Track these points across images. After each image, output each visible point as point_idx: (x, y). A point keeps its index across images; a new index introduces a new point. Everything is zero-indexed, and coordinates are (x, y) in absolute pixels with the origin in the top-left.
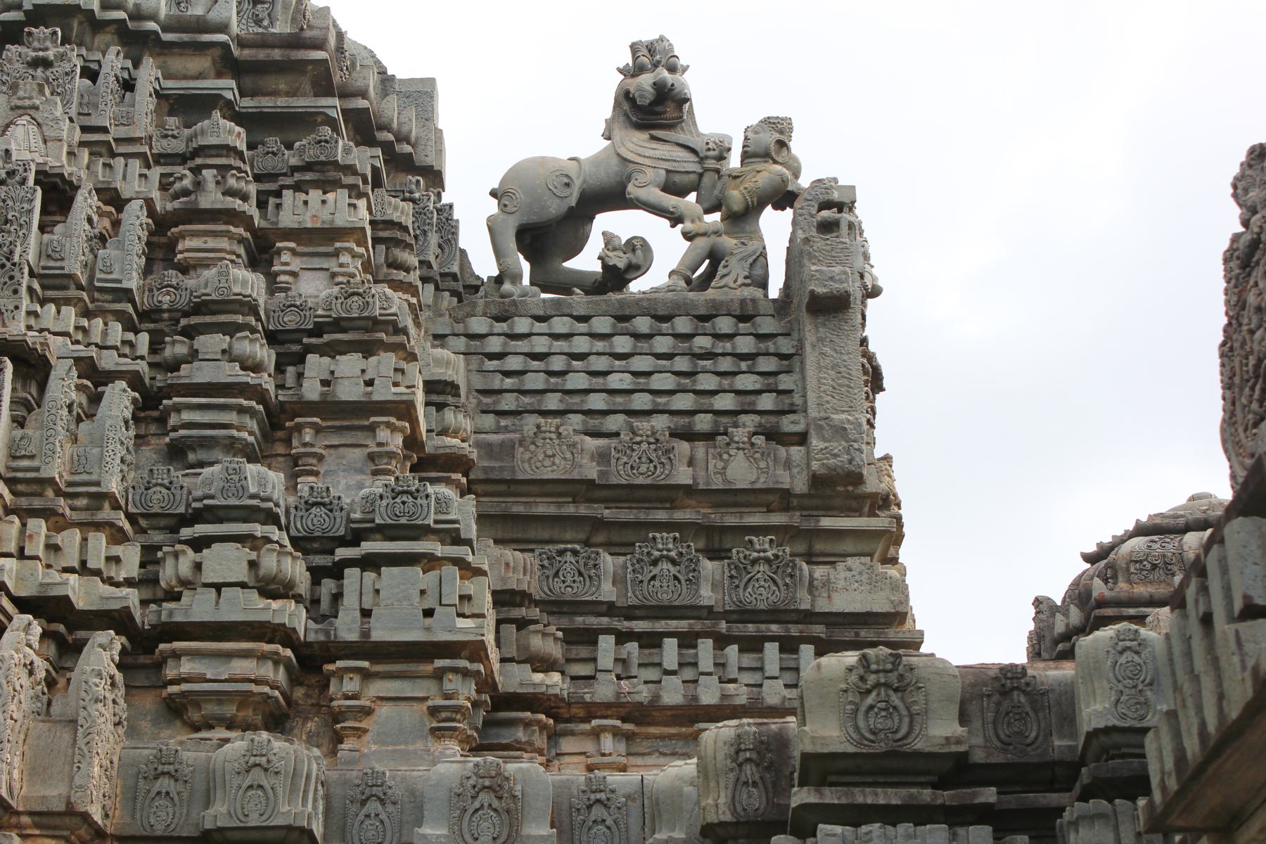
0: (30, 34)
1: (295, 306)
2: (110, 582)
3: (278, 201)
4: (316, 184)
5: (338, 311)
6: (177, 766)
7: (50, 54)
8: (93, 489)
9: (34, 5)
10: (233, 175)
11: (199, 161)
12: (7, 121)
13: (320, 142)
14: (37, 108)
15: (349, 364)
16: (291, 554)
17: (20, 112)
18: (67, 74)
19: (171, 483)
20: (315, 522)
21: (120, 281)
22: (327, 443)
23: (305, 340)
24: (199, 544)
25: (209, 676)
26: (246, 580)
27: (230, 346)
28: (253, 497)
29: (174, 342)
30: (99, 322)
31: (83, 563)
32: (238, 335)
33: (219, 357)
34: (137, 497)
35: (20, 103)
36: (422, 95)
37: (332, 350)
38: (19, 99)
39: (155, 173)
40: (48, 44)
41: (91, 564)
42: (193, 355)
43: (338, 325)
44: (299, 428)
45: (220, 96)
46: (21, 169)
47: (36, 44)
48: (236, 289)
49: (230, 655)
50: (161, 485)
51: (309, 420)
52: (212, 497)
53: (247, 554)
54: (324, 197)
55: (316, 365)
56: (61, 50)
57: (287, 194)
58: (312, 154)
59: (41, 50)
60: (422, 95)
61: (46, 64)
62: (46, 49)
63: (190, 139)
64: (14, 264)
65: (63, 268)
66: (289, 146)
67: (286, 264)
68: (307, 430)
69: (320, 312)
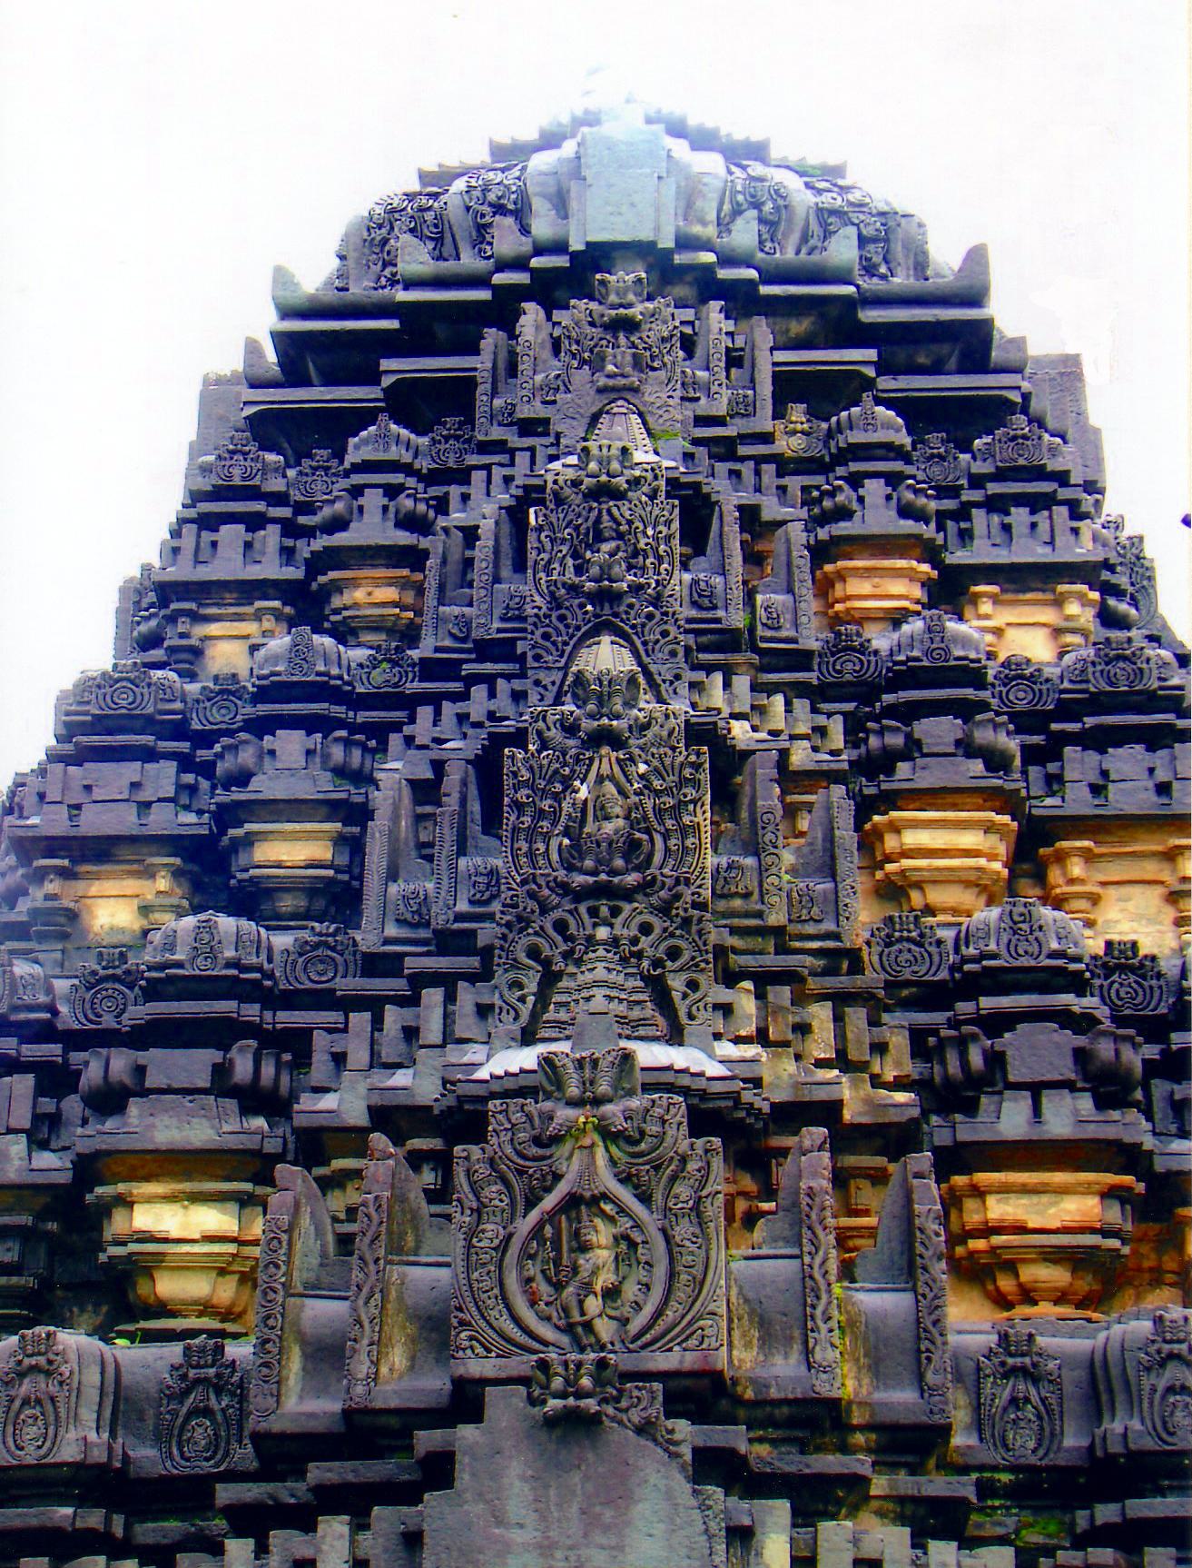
0: (603, 283)
1: (1022, 677)
2: (876, 1082)
3: (464, 489)
4: (1020, 500)
5: (1097, 685)
6: (1036, 1359)
7: (636, 312)
8: (830, 944)
9: (588, 244)
10: (909, 487)
11: (854, 467)
12: (594, 409)
13: (1014, 438)
14: (635, 390)
15: (1127, 761)
16: (1113, 1034)
17: (613, 396)
18: (663, 340)
19: (922, 935)
20: (1122, 994)
21: (794, 641)
22: (1103, 878)
23: (1054, 726)
24: (998, 1024)
25: (1031, 1225)
26: (1073, 1076)
27: (969, 736)
28: (1054, 955)
29: (881, 733)
30: (779, 700)
31: (841, 1053)
32: (978, 717)
33: (951, 749)
34: (875, 959)
35: (611, 382)
36: (1068, 372)
37: (1100, 741)
38: (608, 376)
39: (794, 483)
40: (631, 297)
41: (853, 1054)
42: (912, 749)
43: (1097, 703)
44: (1061, 858)
45: (859, 373)
46: (649, 476)
47: (613, 298)
48: (958, 652)
49: (1064, 1191)
50: (909, 940)
51: (1078, 844)
52: (994, 956)
53: (1069, 1040)
54: (1035, 518)
55: (1078, 764)
56: (650, 306)
57: (978, 515)
58: (1007, 455)
59: (622, 306)
60: (1068, 372)
61: (630, 326)
62: (630, 306)
63: (830, 434)
64: (666, 614)
65: (718, 621)
66: (967, 448)
67: (987, 617)
68: (1075, 860)
69: (1066, 685)
